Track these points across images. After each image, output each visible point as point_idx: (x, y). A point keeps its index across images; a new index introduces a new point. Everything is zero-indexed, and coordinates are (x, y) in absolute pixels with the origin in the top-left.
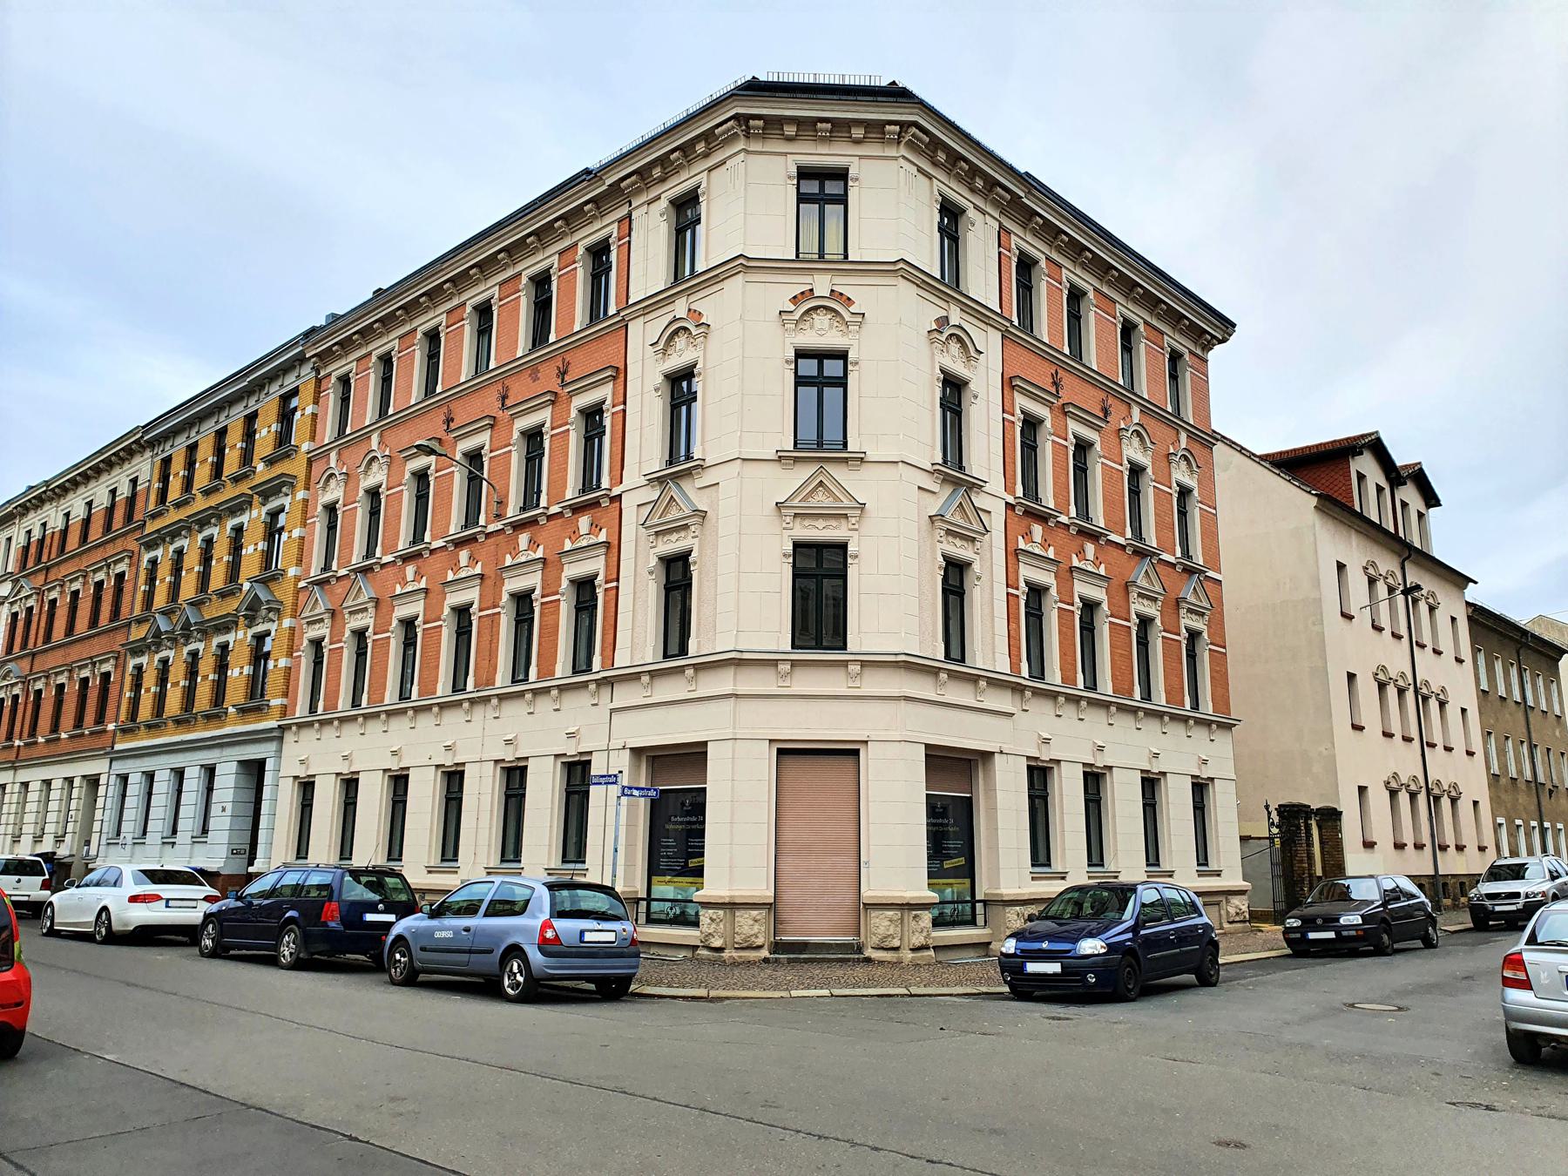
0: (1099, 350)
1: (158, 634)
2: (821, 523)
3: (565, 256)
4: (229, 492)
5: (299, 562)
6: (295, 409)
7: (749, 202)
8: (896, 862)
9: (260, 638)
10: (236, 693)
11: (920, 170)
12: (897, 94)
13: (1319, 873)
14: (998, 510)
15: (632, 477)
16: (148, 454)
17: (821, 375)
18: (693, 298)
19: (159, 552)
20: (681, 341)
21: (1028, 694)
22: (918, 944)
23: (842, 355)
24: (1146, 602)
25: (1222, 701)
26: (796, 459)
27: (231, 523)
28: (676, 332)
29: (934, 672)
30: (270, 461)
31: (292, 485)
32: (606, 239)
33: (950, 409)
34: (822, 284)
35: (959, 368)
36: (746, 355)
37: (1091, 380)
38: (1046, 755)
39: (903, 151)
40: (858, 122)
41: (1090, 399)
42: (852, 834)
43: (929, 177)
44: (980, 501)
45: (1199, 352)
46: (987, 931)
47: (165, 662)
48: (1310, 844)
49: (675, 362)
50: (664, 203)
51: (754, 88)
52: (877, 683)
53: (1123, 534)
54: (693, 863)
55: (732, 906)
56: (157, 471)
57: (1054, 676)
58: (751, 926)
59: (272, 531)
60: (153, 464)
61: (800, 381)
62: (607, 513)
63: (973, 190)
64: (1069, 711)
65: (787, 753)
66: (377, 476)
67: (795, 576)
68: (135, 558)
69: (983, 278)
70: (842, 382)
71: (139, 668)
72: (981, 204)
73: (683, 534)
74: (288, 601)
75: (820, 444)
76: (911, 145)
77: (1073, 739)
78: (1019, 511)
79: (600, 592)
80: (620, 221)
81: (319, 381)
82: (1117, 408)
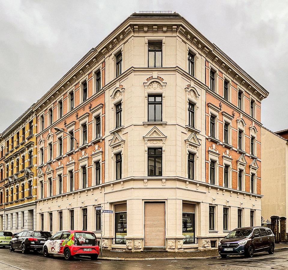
0: (233, 97)
1: (10, 182)
2: (155, 142)
3: (89, 75)
4: (21, 147)
5: (36, 163)
6: (32, 126)
7: (135, 51)
8: (174, 229)
9: (30, 182)
10: (26, 195)
11: (183, 41)
12: (176, 16)
13: (280, 232)
14: (204, 139)
15: (107, 133)
16: (4, 140)
17: (155, 100)
18: (120, 82)
19: (8, 163)
20: (118, 94)
21: (210, 188)
22: (179, 248)
23: (160, 95)
24: (241, 166)
25: (259, 190)
26: (149, 125)
27: (22, 155)
28: (116, 92)
29: (185, 182)
30: (28, 139)
31: (33, 144)
32: (99, 70)
33: (192, 112)
34: (155, 75)
35: (194, 100)
36: (135, 94)
37: (231, 106)
38: (214, 203)
39: (178, 34)
40: (165, 25)
41: (229, 111)
42: (164, 222)
43: (186, 43)
44: (199, 136)
45: (259, 101)
46: (198, 245)
47: (12, 188)
48: (278, 225)
49: (117, 100)
50: (113, 55)
51: (136, 16)
52: (170, 184)
53: (237, 148)
54: (125, 230)
55: (133, 239)
56: (6, 144)
57: (217, 184)
58: (140, 245)
59: (30, 157)
60: (5, 142)
61: (149, 103)
62: (101, 144)
63: (198, 48)
64: (220, 192)
65: (147, 203)
66: (51, 140)
67: (148, 157)
68: (4, 165)
69: (201, 74)
70: (160, 103)
71: (7, 190)
72: (200, 52)
73: (119, 147)
74: (35, 172)
75: (155, 120)
76: (180, 32)
77: (221, 199)
78: (209, 140)
79: (101, 164)
80: (102, 63)
81: (37, 118)
82: (237, 115)
